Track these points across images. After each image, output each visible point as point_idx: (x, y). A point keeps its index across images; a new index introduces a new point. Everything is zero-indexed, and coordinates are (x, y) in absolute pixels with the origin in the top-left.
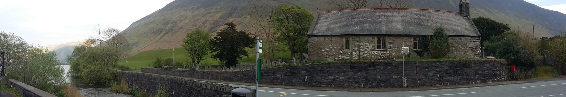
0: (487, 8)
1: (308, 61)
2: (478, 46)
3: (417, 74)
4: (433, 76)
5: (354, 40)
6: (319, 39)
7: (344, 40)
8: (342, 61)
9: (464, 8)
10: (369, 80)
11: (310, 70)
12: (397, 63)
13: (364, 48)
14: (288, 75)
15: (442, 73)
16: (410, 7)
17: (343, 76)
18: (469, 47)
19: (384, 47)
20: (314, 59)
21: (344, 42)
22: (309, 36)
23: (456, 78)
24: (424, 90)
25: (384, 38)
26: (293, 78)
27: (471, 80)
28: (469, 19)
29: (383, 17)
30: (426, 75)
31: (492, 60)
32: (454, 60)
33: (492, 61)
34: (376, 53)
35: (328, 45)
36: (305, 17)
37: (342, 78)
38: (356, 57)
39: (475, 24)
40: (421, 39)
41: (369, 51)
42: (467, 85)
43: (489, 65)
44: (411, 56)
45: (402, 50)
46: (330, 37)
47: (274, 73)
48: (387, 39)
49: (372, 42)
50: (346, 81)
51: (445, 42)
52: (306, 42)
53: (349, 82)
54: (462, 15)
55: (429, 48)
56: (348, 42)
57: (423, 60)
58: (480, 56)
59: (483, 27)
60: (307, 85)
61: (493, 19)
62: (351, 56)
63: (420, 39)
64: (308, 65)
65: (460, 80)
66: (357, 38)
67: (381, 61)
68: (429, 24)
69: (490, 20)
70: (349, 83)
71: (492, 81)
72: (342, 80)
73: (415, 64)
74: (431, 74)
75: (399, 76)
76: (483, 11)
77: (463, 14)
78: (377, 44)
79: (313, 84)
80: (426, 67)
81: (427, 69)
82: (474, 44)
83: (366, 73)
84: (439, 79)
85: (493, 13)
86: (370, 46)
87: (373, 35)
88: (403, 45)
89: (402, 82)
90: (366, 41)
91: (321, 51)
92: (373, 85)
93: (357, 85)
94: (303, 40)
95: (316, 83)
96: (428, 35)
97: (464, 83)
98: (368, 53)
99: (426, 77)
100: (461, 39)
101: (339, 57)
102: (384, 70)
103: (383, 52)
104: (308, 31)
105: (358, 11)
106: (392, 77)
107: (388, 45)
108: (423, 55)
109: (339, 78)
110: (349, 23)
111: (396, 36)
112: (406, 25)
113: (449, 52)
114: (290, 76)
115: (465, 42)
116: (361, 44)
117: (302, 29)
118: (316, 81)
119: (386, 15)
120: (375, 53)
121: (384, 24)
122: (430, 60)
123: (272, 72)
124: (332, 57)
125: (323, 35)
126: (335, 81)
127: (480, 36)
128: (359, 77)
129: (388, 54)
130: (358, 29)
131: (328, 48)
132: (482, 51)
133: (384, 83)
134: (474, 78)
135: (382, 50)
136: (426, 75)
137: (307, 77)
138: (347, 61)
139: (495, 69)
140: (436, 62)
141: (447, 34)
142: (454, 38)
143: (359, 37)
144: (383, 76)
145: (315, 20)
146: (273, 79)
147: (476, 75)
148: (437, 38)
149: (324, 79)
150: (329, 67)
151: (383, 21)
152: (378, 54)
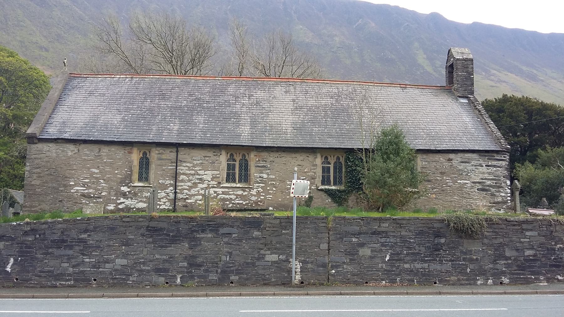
0: (524, 68)
1: (21, 214)
3: (329, 250)
4: (370, 257)
5: (164, 157)
6: (63, 151)
7: (135, 156)
8: (124, 214)
9: (459, 74)
11: (24, 238)
12: (278, 221)
13: (190, 181)
15: (398, 250)
16: (316, 75)
17: (125, 256)
18: (473, 183)
19: (245, 177)
20: (42, 207)
21: (136, 163)
22: (33, 139)
23: (435, 267)
24: (347, 294)
25: (244, 155)
27: (484, 275)
28: (472, 104)
29: (246, 101)
30: (352, 253)
31: (545, 220)
32: (432, 216)
33: (548, 223)
34: (223, 193)
35: (89, 168)
36: (26, 84)
38: (164, 205)
39: (490, 116)
40: (342, 160)
41: (202, 189)
42: (468, 286)
43: (539, 234)
44: (316, 202)
45: (293, 186)
46: (96, 148)
48: (253, 159)
49: (213, 166)
50: (131, 269)
51: (406, 168)
52: (23, 157)
53: (142, 271)
54: (453, 94)
55: (362, 183)
56: (145, 164)
57: (344, 214)
58: (509, 208)
59: (513, 123)
60: (11, 285)
61: (547, 98)
62: (152, 200)
63: (338, 158)
64: (19, 224)
65: (447, 272)
67: (233, 214)
68: (364, 120)
69: (537, 103)
70: (140, 275)
71: (548, 280)
72: (120, 267)
73: (324, 225)
74: (366, 252)
75: (281, 257)
76: (512, 78)
77: (457, 90)
78: (226, 171)
79: (31, 280)
80: (354, 235)
81: (356, 240)
82: (489, 174)
83: (190, 248)
84: (389, 268)
85: (542, 81)
86: (208, 175)
88: (296, 176)
89: (289, 271)
90: (195, 162)
92: (210, 278)
94: (14, 149)
95: (40, 276)
96: (362, 149)
97: (459, 280)
98: (201, 194)
99: (354, 260)
100: (452, 160)
101: (119, 202)
102: (240, 240)
103: (240, 192)
104: (30, 125)
105: (178, 80)
106: (263, 258)
107: (254, 173)
108: (346, 200)
109: (113, 261)
110: (151, 110)
112: (303, 122)
113: (416, 196)
115: (460, 168)
116: (182, 169)
117: (15, 117)
118: (41, 272)
119: (252, 96)
120: (218, 195)
121: (246, 118)
122: (364, 214)
124: (97, 202)
126: (101, 269)
127: (507, 151)
129: (254, 198)
130: (176, 128)
131: (87, 178)
132: (512, 194)
133: (238, 273)
134: (491, 268)
135: (238, 185)
136: (352, 253)
137: (12, 260)
138: (140, 214)
139: (556, 245)
140: (380, 220)
141: (411, 147)
142: (431, 157)
143: (177, 152)
144: (238, 255)
145: (54, 94)
147: (495, 261)
148: (385, 157)
149: (66, 265)
150: (86, 231)
152: (227, 196)
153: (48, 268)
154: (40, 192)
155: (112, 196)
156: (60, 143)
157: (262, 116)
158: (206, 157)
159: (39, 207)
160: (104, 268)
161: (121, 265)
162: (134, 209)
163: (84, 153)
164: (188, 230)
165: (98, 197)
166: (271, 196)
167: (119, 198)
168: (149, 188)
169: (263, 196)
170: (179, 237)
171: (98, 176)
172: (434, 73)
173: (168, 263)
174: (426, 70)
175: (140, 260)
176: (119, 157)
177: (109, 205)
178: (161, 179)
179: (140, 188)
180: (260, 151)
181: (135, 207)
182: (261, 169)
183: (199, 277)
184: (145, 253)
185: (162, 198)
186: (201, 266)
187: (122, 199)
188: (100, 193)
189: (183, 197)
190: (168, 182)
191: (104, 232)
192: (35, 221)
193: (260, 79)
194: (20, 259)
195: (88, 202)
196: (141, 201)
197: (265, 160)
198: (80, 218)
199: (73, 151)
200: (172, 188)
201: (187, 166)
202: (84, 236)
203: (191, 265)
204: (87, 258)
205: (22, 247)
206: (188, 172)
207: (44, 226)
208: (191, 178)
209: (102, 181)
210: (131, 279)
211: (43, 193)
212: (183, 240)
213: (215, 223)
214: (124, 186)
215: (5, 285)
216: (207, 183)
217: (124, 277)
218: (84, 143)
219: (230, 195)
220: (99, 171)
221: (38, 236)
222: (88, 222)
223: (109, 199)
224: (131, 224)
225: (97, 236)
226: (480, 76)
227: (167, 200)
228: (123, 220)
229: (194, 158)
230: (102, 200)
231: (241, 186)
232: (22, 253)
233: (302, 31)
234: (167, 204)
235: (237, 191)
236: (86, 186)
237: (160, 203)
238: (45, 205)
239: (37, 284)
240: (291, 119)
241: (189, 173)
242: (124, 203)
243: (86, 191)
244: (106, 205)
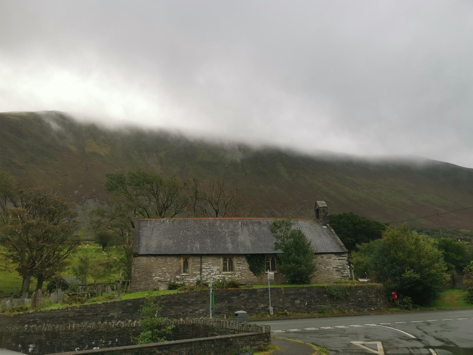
2: (346, 265)
7: (182, 261)
13: (207, 272)
19: (232, 269)
21: (182, 264)
35: (161, 268)
63: (273, 258)
66: (198, 258)
74: (298, 302)
75: (265, 305)
86: (215, 268)
87: (218, 255)
90: (209, 262)
100: (323, 257)
107: (236, 267)
115: (327, 261)
116: (204, 266)
130: (198, 246)
131: (160, 272)
132: (351, 271)
135: (229, 273)
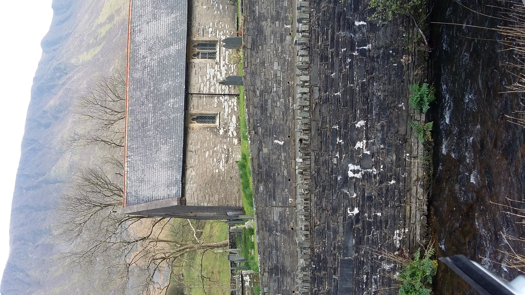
7: (195, 125)
10: (278, 13)
13: (215, 85)
14: (274, 190)
17: (272, 64)
19: (212, 44)
20: (236, 192)
26: (278, 174)
34: (224, 60)
35: (205, 159)
37: (276, 66)
46: (189, 154)
47: (270, 231)
48: (197, 38)
50: (281, 59)
56: (202, 118)
64: (250, 138)
72: (280, 67)
78: (207, 60)
90: (200, 81)
91: (219, 176)
92: (286, 5)
93: (287, 37)
95: (287, 120)
101: (231, 136)
107: (209, 37)
111: (191, 21)
114: (275, 183)
116: (205, 90)
118: (283, 120)
120: (226, 64)
121: (164, 53)
123: (268, 234)
124: (232, 152)
125: (181, 168)
126: (281, 79)
128: (273, 32)
131: (213, 160)
135: (218, 49)
137: (276, 141)
146: (284, 231)
149: (278, 103)
150: (254, 91)
151: (156, 57)
152: (227, 57)
153: (281, 116)
154: (224, 194)
155: (227, 141)
156: (185, 181)
157: (161, 41)
158: (196, 73)
159: (236, 194)
160: (280, 77)
161: (278, 65)
162: (237, 124)
163: (193, 163)
164: (254, 22)
165: (228, 151)
166: (226, 25)
167: (228, 135)
168: (221, 114)
169: (226, 31)
170: (258, 28)
171: (211, 151)
172: (102, 45)
173: (276, 34)
174: (98, 52)
175: (275, 53)
176: (196, 137)
177: (234, 143)
178: (214, 106)
179: (221, 120)
180: (190, 33)
181: (236, 124)
182: (205, 33)
183: (286, 13)
184: (270, 50)
185: (229, 104)
186: (278, 12)
187: (229, 133)
188: (225, 150)
189: (228, 89)
190: (216, 100)
191: (255, 79)
192: (248, 128)
193: (129, 56)
194: (274, 136)
195: (232, 158)
196: (231, 120)
197: (198, 30)
198: (245, 96)
199: (191, 171)
200: (221, 98)
201: (203, 87)
202: (258, 93)
203: (278, 19)
204: (274, 89)
205: (266, 135)
206: (208, 86)
207: (251, 121)
208: (212, 84)
209: (215, 149)
210: (287, 58)
211: (225, 192)
212: (261, 25)
213: (248, 4)
214: (219, 133)
215: (293, 144)
216: (217, 72)
217: (286, 63)
218: (185, 163)
219: (225, 55)
220: (207, 152)
221: (258, 125)
222: (248, 90)
223: (229, 143)
224: (249, 61)
225: (258, 83)
226: (106, 2)
227: (230, 101)
228: (246, 66)
229: (197, 82)
230: (230, 148)
231: (219, 47)
232: (271, 135)
233: (57, 171)
234: (233, 101)
235: (222, 50)
236: (219, 160)
237: (232, 106)
238: (234, 190)
239: (292, 122)
240: (164, 18)
241: (209, 85)
242: (232, 132)
243: (223, 160)
244: (234, 145)
